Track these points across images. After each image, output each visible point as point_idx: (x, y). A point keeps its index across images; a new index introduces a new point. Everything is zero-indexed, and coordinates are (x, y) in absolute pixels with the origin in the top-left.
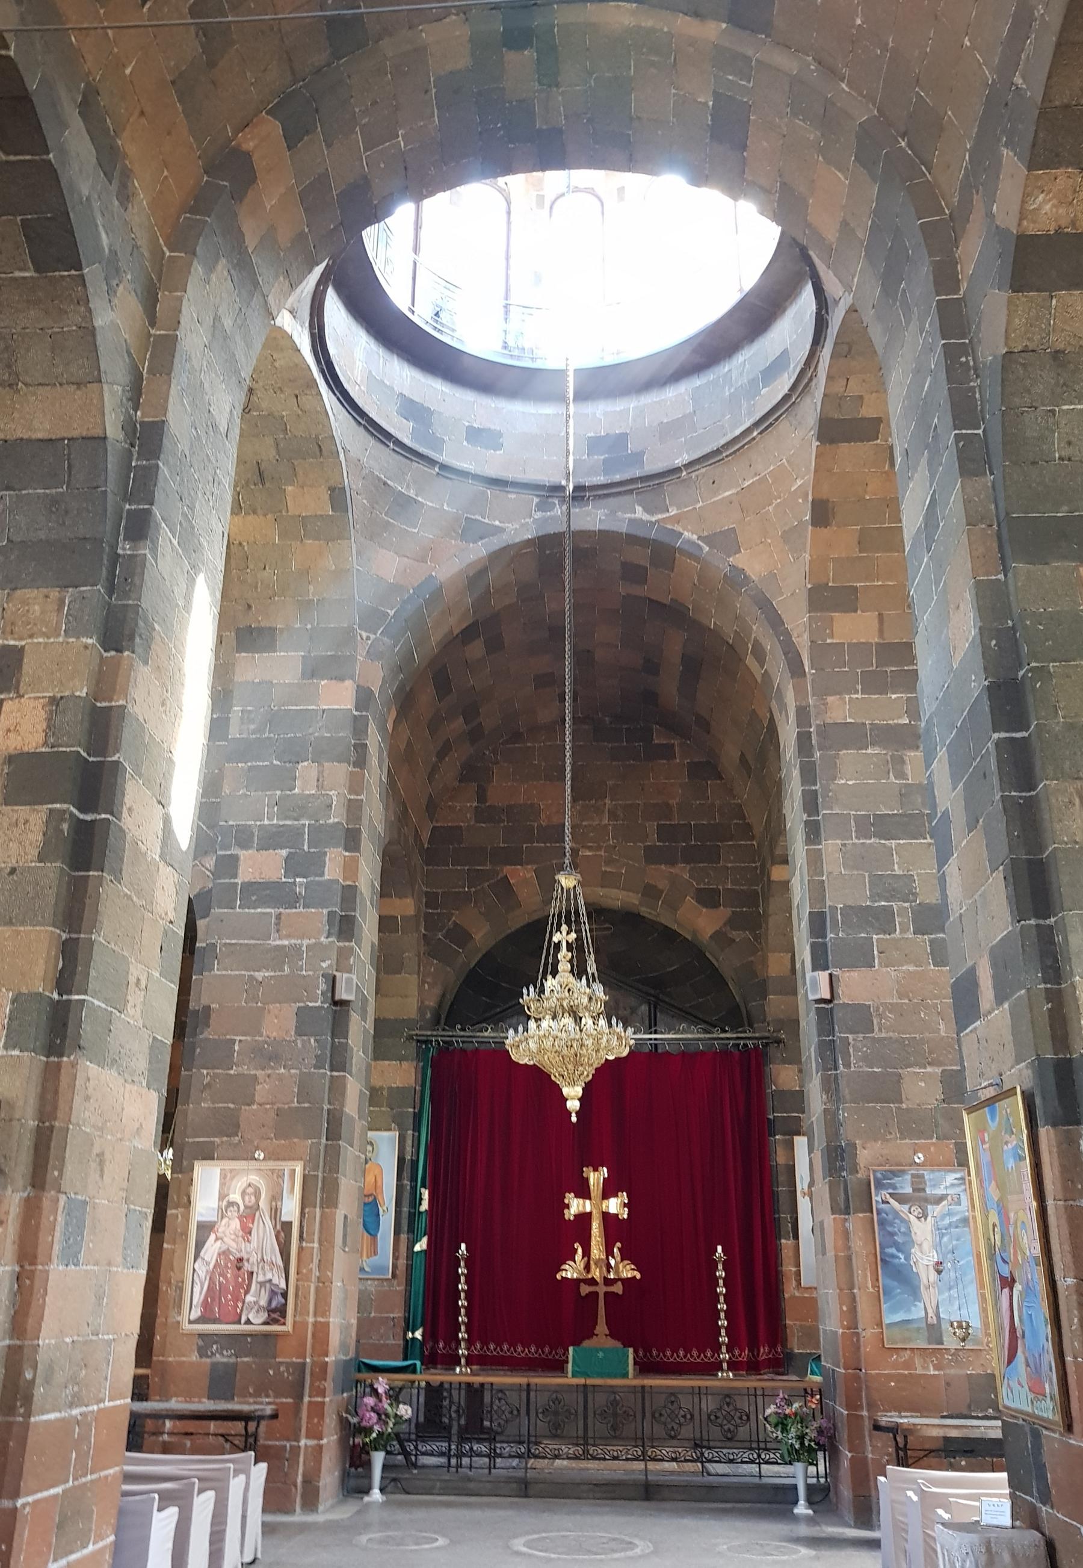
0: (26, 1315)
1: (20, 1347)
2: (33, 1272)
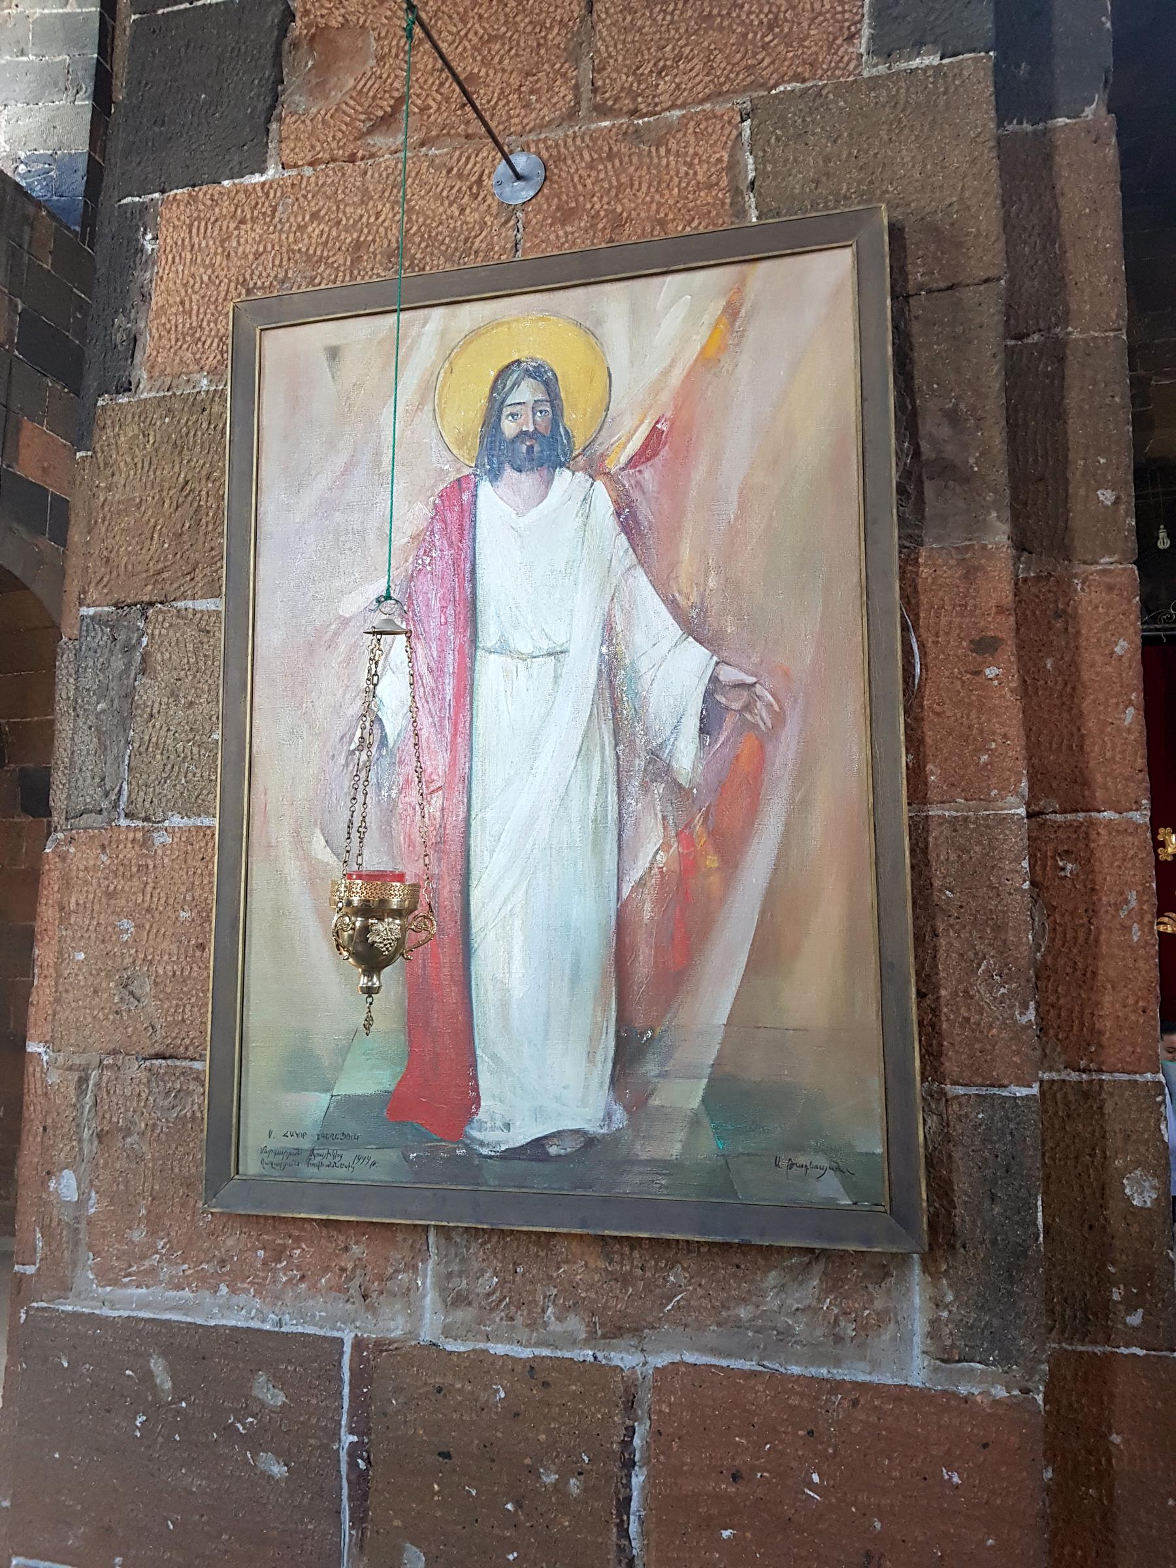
0: (1087, 979)
1: (1089, 1094)
2: (1084, 833)
